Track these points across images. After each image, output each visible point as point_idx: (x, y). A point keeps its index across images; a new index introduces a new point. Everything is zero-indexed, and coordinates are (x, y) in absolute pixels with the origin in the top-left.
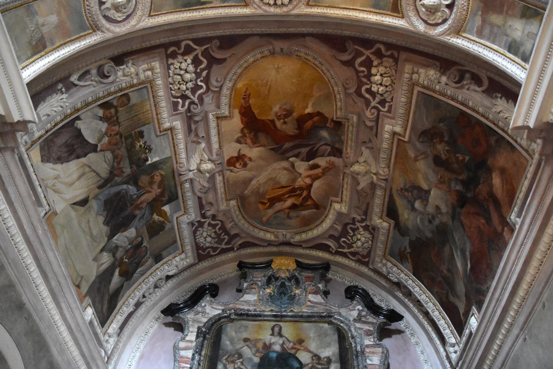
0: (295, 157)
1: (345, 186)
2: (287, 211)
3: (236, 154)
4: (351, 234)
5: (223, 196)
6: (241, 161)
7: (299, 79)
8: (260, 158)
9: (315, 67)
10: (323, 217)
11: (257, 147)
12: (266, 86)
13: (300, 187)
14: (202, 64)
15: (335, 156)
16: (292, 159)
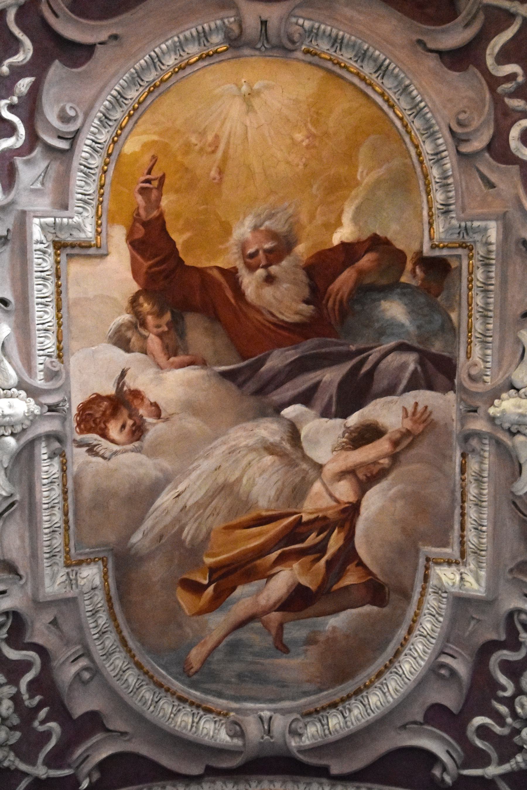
1: (472, 490)
2: (275, 616)
3: (110, 389)
4: (504, 689)
5: (58, 541)
6: (125, 413)
7: (313, 130)
9: (362, 85)
10: (402, 632)
11: (182, 365)
12: (213, 152)
13: (316, 519)
14: (16, 52)
15: (430, 387)
16: (290, 412)
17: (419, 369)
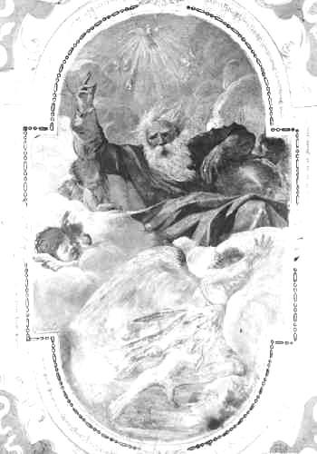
0: (187, 236)
7: (193, 56)
8: (110, 238)
12: (128, 70)
15: (272, 224)
17: (265, 213)
